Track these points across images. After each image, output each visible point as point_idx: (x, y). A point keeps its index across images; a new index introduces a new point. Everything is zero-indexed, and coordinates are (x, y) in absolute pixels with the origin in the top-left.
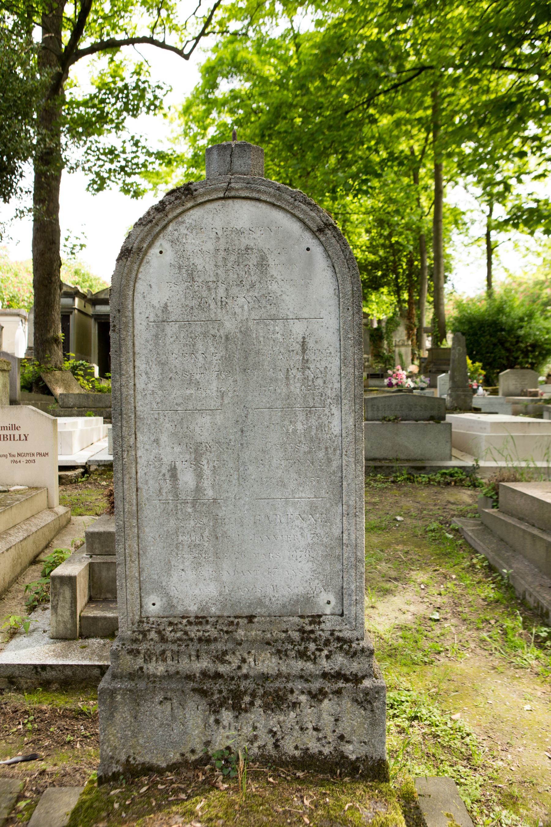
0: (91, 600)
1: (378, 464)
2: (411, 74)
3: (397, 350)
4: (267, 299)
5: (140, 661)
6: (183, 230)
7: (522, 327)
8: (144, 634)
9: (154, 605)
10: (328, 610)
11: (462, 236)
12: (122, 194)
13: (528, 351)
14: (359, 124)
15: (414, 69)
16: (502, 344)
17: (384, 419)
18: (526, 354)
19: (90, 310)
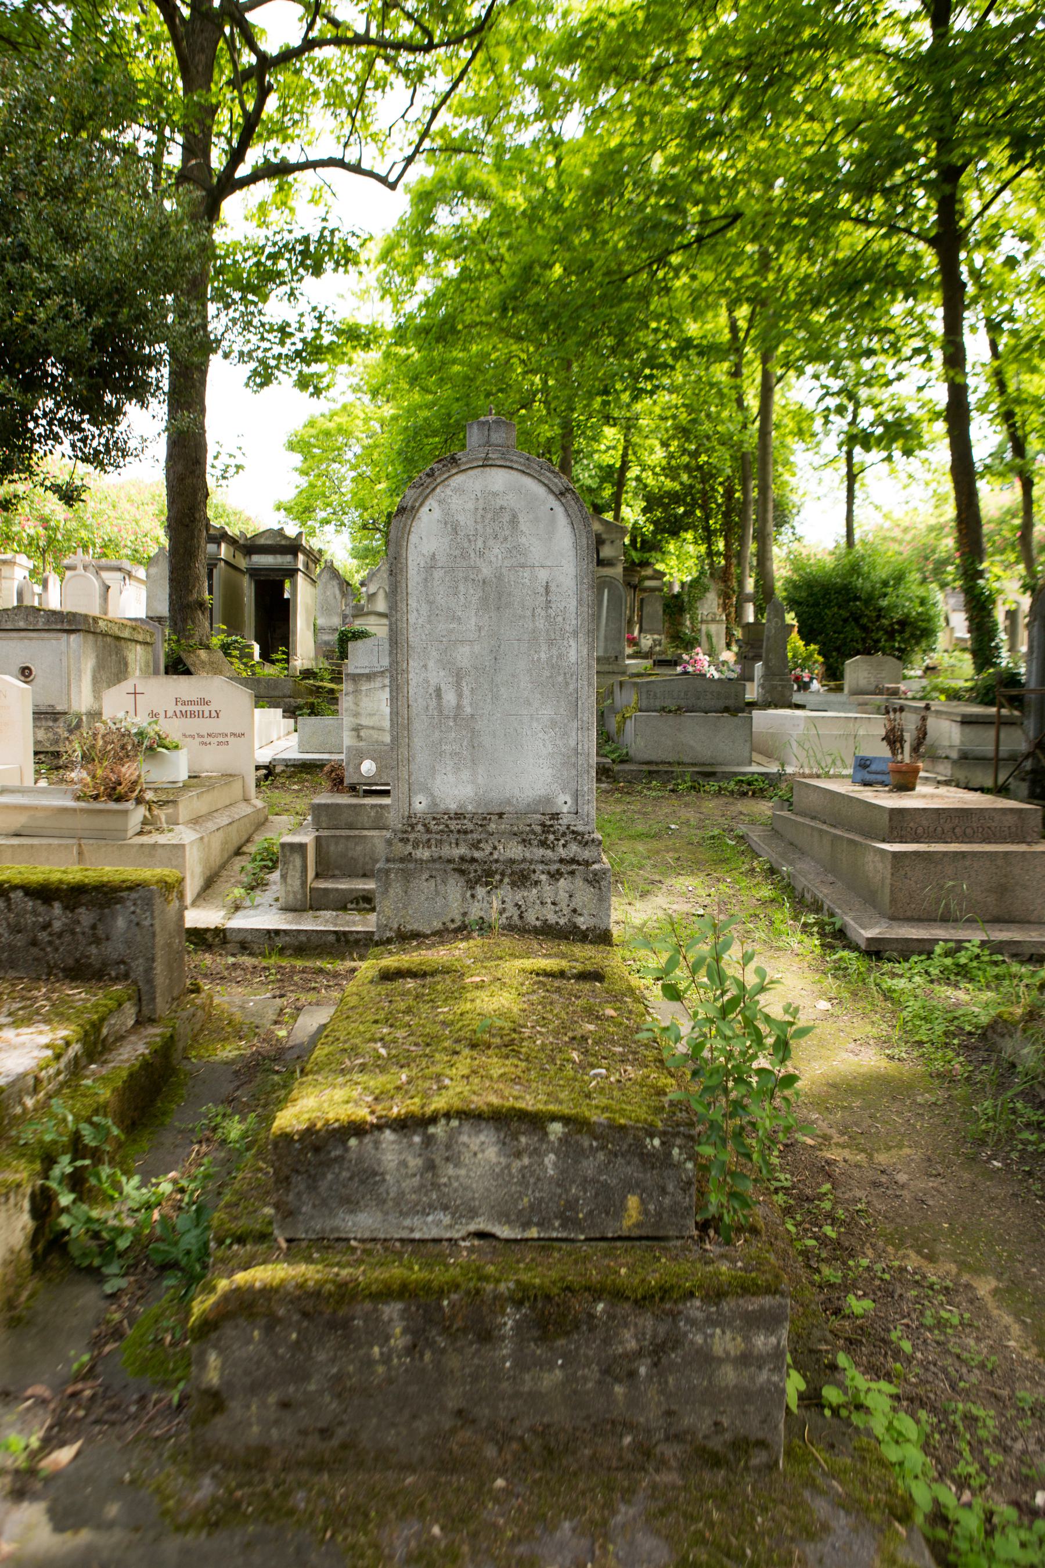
0: (317, 876)
1: (654, 768)
2: (723, 222)
3: (704, 627)
4: (516, 550)
5: (409, 848)
6: (448, 492)
7: (885, 595)
8: (412, 826)
9: (420, 804)
10: (565, 809)
11: (810, 453)
12: (296, 390)
13: (894, 631)
14: (644, 297)
15: (725, 216)
16: (857, 620)
17: (663, 709)
18: (891, 635)
19: (243, 563)
